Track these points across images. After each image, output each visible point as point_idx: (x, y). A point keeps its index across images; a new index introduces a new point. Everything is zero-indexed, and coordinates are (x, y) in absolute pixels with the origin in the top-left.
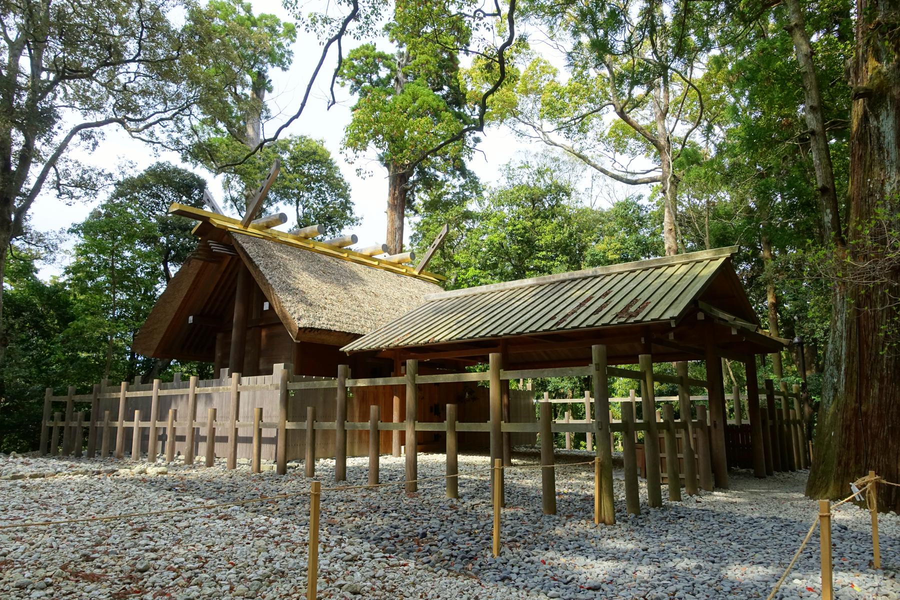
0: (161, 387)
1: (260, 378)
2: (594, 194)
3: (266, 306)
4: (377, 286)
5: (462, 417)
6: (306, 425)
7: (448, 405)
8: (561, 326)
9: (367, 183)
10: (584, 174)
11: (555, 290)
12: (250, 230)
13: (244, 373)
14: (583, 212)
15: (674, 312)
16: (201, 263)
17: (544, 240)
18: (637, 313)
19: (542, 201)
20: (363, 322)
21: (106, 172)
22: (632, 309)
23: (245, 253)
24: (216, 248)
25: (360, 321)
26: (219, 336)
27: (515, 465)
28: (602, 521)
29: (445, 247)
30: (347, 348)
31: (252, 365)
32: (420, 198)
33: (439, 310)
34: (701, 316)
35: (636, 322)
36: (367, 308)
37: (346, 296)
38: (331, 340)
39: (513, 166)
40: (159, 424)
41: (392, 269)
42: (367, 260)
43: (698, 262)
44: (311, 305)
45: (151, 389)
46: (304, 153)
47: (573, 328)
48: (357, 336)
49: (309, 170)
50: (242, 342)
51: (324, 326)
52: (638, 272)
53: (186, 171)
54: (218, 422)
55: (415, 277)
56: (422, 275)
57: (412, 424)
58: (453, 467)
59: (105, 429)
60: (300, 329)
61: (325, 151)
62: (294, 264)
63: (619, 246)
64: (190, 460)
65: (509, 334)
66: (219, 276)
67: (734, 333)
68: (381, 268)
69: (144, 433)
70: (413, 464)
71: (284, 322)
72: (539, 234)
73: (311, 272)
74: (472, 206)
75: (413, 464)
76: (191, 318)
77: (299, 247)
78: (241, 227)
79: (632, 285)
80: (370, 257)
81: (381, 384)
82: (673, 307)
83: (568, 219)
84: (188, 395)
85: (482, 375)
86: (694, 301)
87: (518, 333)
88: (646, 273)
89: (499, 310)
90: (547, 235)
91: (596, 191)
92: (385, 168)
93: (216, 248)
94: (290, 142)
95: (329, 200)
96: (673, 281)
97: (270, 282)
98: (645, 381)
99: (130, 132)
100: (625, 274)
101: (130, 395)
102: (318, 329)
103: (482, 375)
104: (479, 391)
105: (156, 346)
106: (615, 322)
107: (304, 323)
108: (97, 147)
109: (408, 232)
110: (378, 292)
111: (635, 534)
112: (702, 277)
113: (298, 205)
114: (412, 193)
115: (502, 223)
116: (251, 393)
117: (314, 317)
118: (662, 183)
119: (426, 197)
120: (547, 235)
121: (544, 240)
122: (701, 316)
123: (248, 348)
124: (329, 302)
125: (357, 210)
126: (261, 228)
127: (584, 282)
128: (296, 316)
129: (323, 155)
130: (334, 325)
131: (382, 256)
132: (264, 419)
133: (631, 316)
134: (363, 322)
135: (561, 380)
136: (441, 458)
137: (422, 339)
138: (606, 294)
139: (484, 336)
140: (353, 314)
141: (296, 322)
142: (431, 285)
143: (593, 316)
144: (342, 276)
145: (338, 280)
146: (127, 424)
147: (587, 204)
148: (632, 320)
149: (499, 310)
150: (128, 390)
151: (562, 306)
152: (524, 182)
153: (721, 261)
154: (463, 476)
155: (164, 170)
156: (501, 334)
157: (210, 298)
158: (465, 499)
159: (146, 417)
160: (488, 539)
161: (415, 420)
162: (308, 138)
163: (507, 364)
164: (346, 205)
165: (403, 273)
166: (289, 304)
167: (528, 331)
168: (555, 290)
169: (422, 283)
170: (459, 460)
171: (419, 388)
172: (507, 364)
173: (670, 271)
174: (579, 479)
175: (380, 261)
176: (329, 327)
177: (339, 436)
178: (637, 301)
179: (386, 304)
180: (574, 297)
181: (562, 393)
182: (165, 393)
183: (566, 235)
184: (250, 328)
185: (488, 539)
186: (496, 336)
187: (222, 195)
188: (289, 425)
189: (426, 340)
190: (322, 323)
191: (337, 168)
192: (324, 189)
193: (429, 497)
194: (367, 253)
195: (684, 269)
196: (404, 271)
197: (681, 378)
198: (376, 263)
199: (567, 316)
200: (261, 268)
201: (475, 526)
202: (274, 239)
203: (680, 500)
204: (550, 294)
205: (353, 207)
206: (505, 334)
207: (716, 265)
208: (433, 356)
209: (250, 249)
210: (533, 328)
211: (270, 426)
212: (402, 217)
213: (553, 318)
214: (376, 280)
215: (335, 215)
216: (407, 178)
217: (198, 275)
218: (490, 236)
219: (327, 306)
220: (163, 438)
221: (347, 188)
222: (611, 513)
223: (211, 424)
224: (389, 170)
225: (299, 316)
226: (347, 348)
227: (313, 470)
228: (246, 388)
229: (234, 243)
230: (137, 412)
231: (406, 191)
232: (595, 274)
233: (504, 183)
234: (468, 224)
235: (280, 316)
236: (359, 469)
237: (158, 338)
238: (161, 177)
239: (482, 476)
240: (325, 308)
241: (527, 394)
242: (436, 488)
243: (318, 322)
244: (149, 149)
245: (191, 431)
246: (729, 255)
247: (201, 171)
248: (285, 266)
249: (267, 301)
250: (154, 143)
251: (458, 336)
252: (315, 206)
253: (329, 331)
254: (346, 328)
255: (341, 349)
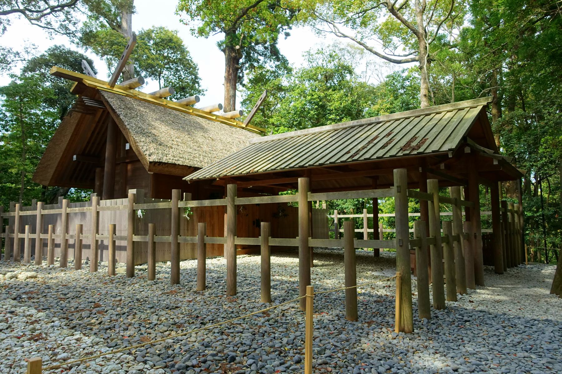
0: (43, 208)
1: (119, 201)
2: (368, 75)
3: (127, 147)
4: (218, 138)
5: (274, 233)
6: (148, 238)
7: (262, 223)
8: (356, 158)
9: (208, 56)
10: (360, 62)
11: (348, 133)
12: (115, 89)
13: (101, 196)
14: (362, 85)
15: (452, 144)
16: (79, 115)
17: (334, 105)
18: (419, 147)
19: (334, 76)
20: (201, 159)
21: (14, 50)
22: (414, 144)
23: (110, 105)
24: (88, 102)
25: (199, 158)
26: (98, 170)
27: (316, 266)
28: (402, 330)
29: (265, 108)
30: (188, 178)
31: (115, 192)
32: (247, 76)
33: (260, 149)
34: (467, 150)
35: (419, 153)
36: (205, 148)
37: (189, 139)
38: (176, 172)
39: (312, 52)
40: (43, 236)
41: (225, 122)
42: (208, 115)
43: (460, 110)
44: (160, 145)
45: (35, 209)
46: (163, 40)
47: (365, 159)
48: (196, 169)
49: (166, 51)
50: (113, 175)
51: (170, 161)
52: (412, 118)
53: (77, 53)
54: (84, 235)
55: (243, 128)
56: (248, 127)
57: (232, 239)
58: (267, 269)
59: (6, 240)
60: (150, 162)
61: (179, 39)
62: (151, 116)
63: (389, 106)
64: (64, 264)
65: (313, 165)
66: (94, 125)
67: (496, 163)
68: (218, 121)
69: (33, 241)
70: (233, 267)
71: (140, 158)
72: (329, 101)
73: (163, 121)
74: (285, 82)
75: (233, 267)
76: (75, 157)
77: (156, 103)
78: (109, 87)
79: (409, 127)
80: (210, 113)
81: (206, 205)
82: (447, 142)
83: (351, 89)
84: (61, 214)
85: (296, 198)
86: (464, 138)
87: (320, 165)
88: (418, 120)
89: (304, 148)
90: (336, 101)
91: (369, 73)
92: (222, 53)
93: (88, 102)
94: (153, 31)
95: (183, 76)
96: (444, 123)
97: (128, 127)
98: (433, 202)
99: (30, 20)
100: (402, 120)
101: (22, 213)
102: (165, 163)
103: (296, 198)
104: (289, 210)
105: (50, 178)
106: (400, 154)
107: (154, 158)
108: (6, 32)
109: (239, 99)
110: (215, 137)
111: (432, 344)
112: (467, 119)
113: (160, 79)
114: (242, 71)
115: (303, 93)
116: (113, 212)
117: (162, 154)
118: (420, 62)
119: (251, 77)
120: (336, 101)
121: (334, 105)
122: (467, 150)
123: (117, 179)
124: (175, 143)
125: (203, 84)
126: (125, 89)
127: (370, 127)
128: (147, 153)
129: (177, 42)
130: (178, 160)
131: (221, 113)
132: (117, 233)
133: (414, 149)
134: (201, 159)
135: (347, 202)
136: (257, 260)
137: (244, 170)
138: (389, 134)
139: (293, 167)
140: (194, 152)
141: (147, 157)
142: (254, 134)
143: (381, 150)
144: (187, 125)
145: (183, 128)
146: (21, 236)
147: (362, 80)
148: (415, 152)
149: (304, 148)
150: (21, 209)
151: (354, 144)
152: (320, 64)
153: (480, 108)
154: (275, 277)
155: (61, 51)
156: (307, 165)
157: (88, 143)
158: (277, 302)
159: (33, 231)
160: (299, 362)
161: (234, 236)
162: (166, 29)
163: (313, 188)
164: (195, 81)
165: (234, 126)
166: (142, 144)
167: (328, 162)
168: (348, 133)
169: (248, 133)
170: (272, 261)
171: (237, 208)
172: (313, 188)
173: (438, 116)
174: (367, 277)
175: (217, 116)
176: (174, 161)
177: (173, 247)
178: (416, 138)
179: (220, 146)
180: (363, 137)
181: (343, 207)
182: (46, 212)
183: (349, 102)
184: (119, 164)
185: (299, 362)
186: (303, 166)
187: (102, 70)
188: (136, 238)
189: (248, 171)
190: (169, 158)
191: (188, 52)
192: (179, 68)
193: (245, 302)
194: (208, 110)
195: (449, 115)
196: (235, 124)
197: (456, 199)
198: (214, 118)
199: (359, 151)
200: (121, 117)
201: (285, 340)
202: (135, 97)
203: (456, 301)
204: (343, 136)
205: (200, 81)
206: (310, 165)
207: (475, 112)
208: (249, 183)
209: (114, 103)
210: (332, 160)
211: (122, 238)
212: (235, 89)
213: (348, 152)
214: (214, 128)
215: (187, 88)
216: (236, 54)
217: (77, 125)
218: (296, 103)
219: (174, 146)
220: (45, 245)
221: (195, 68)
222: (410, 322)
223: (79, 237)
224: (225, 54)
225: (150, 153)
226: (188, 178)
227: (154, 273)
228: (103, 209)
229: (102, 99)
230: (27, 227)
231: (237, 69)
232: (377, 121)
233: (306, 66)
234: (280, 94)
235: (137, 153)
236: (189, 272)
237: (51, 172)
238: (59, 56)
239: (291, 277)
240: (172, 148)
241: (322, 211)
242: (253, 291)
243: (165, 158)
244: (44, 33)
245: (64, 241)
246: (485, 103)
247: (89, 53)
248: (142, 116)
249: (127, 143)
250: (49, 28)
251: (273, 168)
252: (173, 81)
253: (174, 165)
254: (187, 163)
255: (184, 179)
